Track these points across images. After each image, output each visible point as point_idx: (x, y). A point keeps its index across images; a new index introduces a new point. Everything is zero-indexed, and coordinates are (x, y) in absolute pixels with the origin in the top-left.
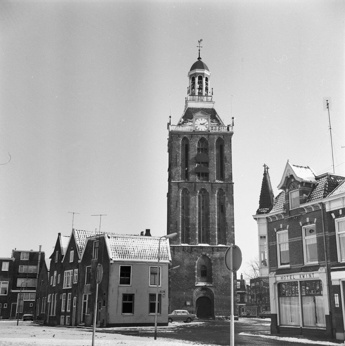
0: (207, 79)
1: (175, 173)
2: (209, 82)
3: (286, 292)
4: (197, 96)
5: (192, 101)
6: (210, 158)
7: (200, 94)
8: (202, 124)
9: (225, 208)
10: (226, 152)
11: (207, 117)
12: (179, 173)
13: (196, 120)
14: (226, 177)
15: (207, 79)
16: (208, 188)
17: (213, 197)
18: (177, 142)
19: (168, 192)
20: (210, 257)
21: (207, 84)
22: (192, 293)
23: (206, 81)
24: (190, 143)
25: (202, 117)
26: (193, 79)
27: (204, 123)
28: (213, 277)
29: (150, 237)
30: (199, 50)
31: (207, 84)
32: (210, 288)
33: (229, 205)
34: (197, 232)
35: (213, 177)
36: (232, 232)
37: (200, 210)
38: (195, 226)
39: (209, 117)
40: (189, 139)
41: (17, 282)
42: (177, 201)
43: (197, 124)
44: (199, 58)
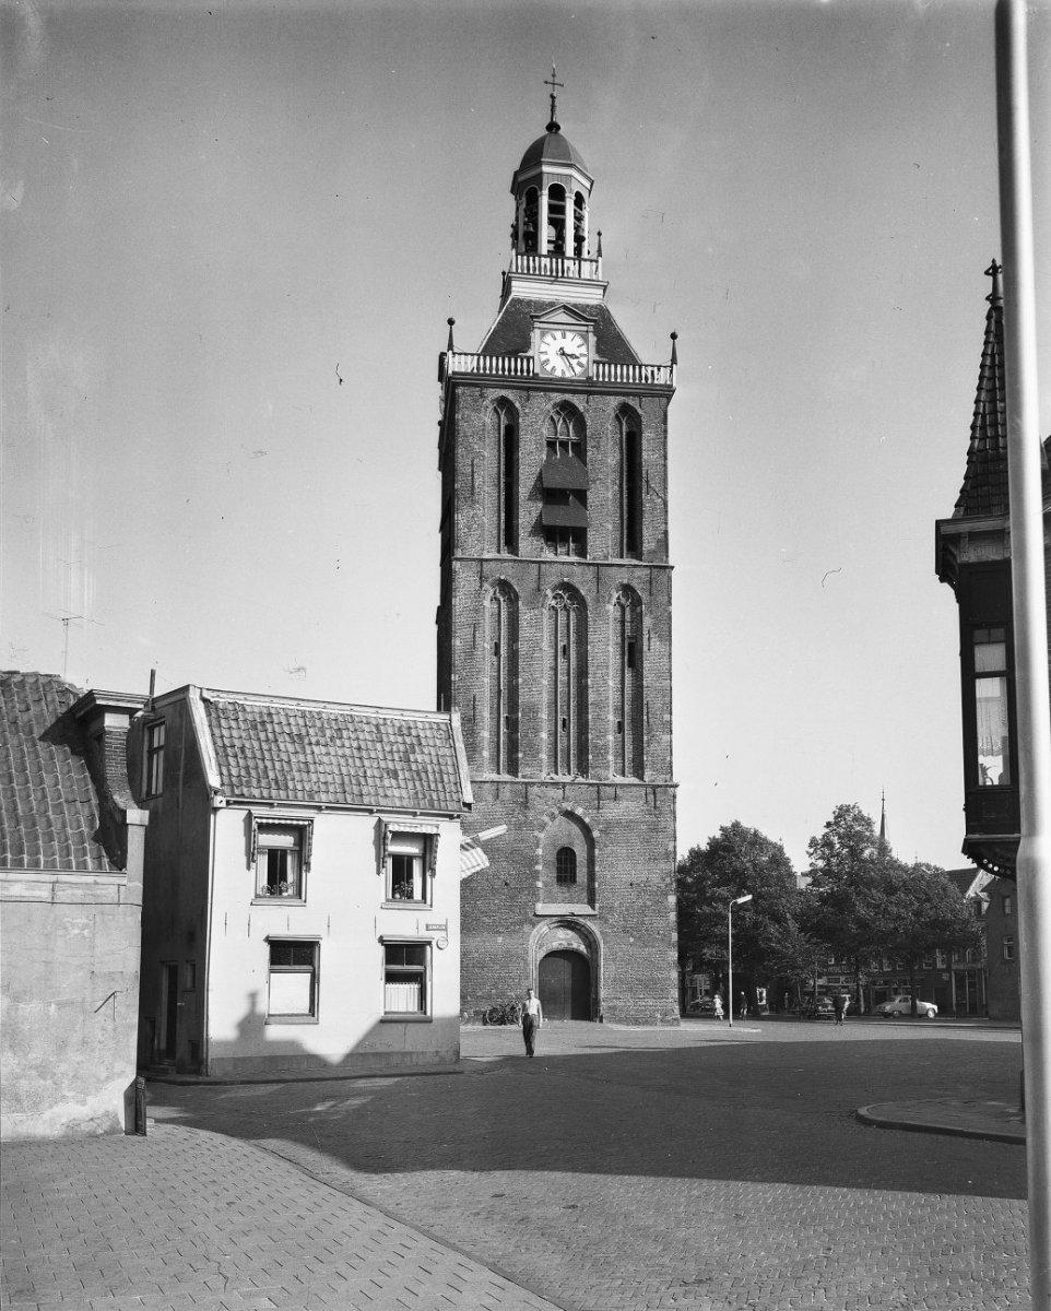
0: (579, 201)
1: (469, 529)
2: (586, 213)
3: (930, 949)
4: (545, 256)
5: (528, 273)
6: (592, 476)
7: (558, 250)
8: (563, 354)
9: (641, 652)
10: (648, 455)
11: (585, 328)
12: (481, 526)
13: (543, 335)
14: (648, 544)
15: (579, 201)
16: (584, 582)
17: (601, 615)
18: (474, 416)
19: (439, 604)
20: (587, 820)
21: (579, 218)
22: (526, 937)
23: (575, 204)
24: (520, 420)
25: (565, 327)
26: (533, 199)
27: (572, 356)
28: (597, 886)
29: (141, 1138)
30: (553, 97)
31: (579, 218)
32: (589, 923)
33: (656, 644)
34: (544, 735)
35: (603, 536)
36: (666, 738)
37: (556, 659)
38: (537, 712)
39: (591, 328)
40: (517, 405)
41: (977, 689)
42: (475, 627)
43: (546, 353)
44: (553, 127)
